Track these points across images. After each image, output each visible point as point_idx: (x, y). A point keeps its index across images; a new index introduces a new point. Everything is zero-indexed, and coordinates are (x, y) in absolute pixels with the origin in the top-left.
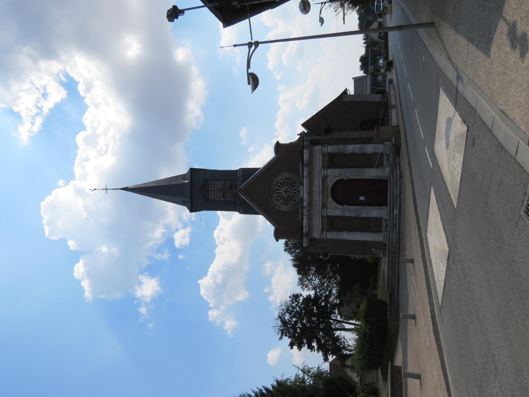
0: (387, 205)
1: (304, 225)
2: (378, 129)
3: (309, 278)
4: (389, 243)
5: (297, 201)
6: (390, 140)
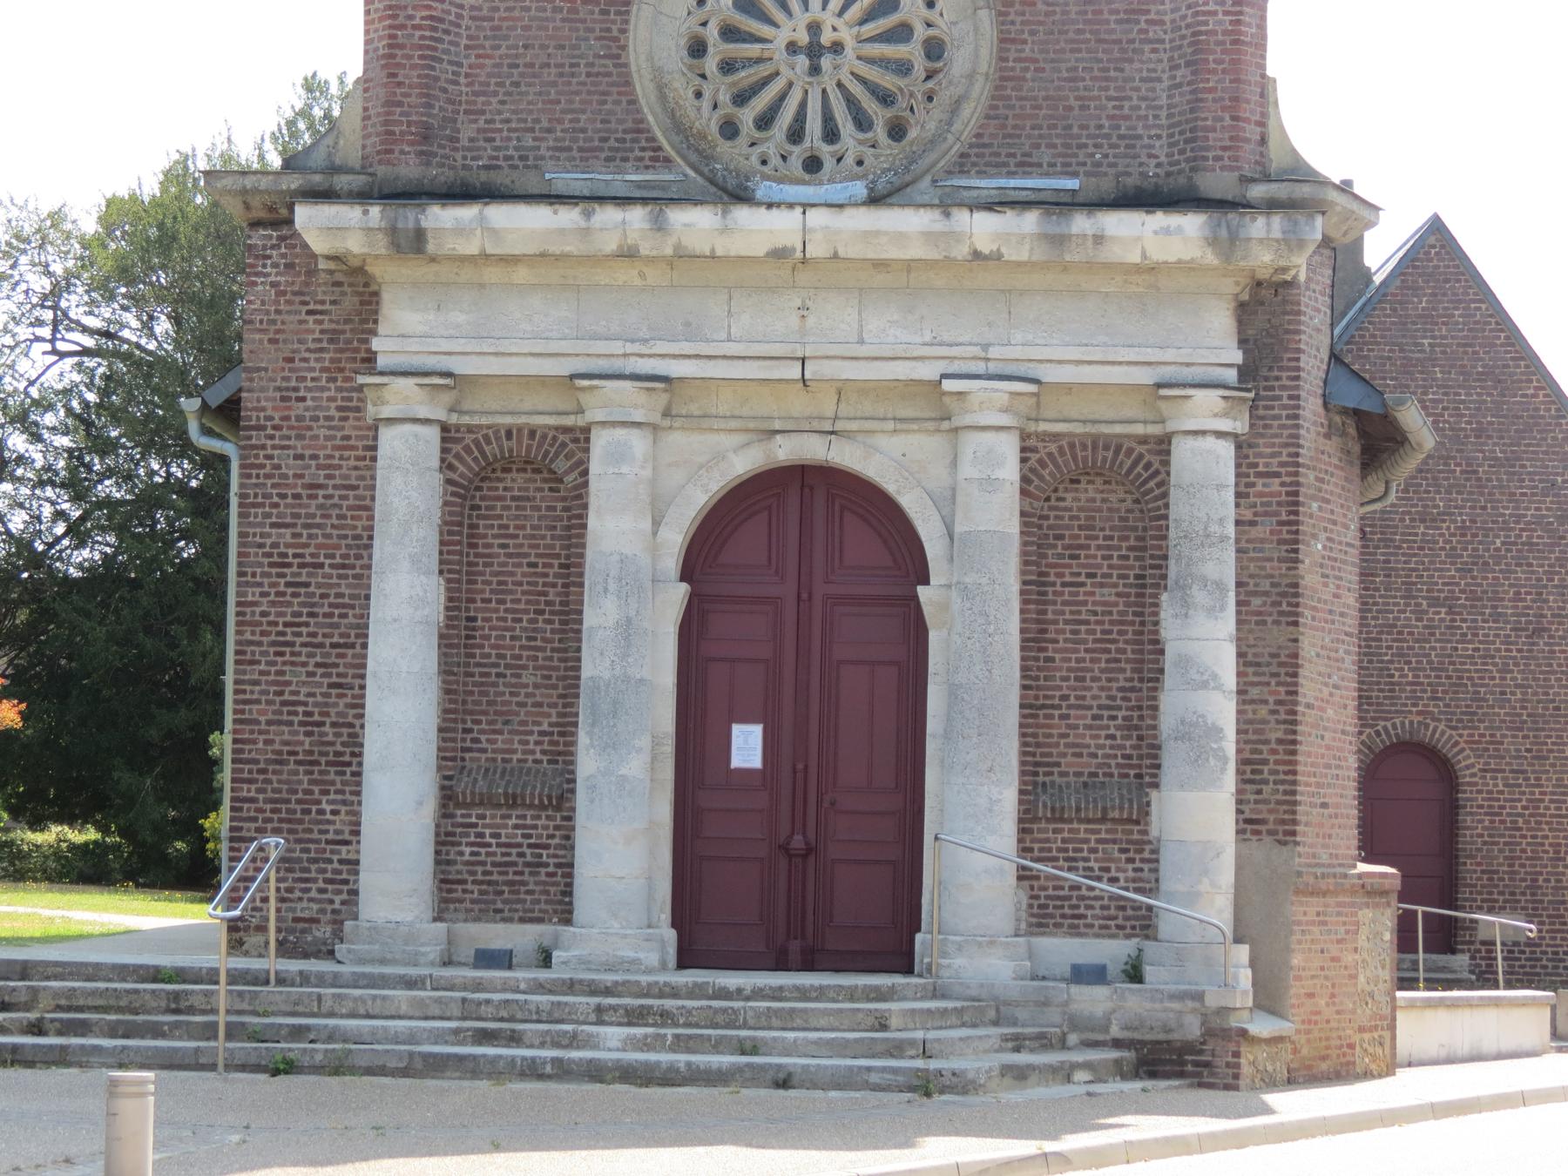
0: (683, 963)
1: (499, 214)
2: (1371, 891)
3: (74, 303)
4: (336, 980)
5: (724, 147)
6: (1268, 998)
